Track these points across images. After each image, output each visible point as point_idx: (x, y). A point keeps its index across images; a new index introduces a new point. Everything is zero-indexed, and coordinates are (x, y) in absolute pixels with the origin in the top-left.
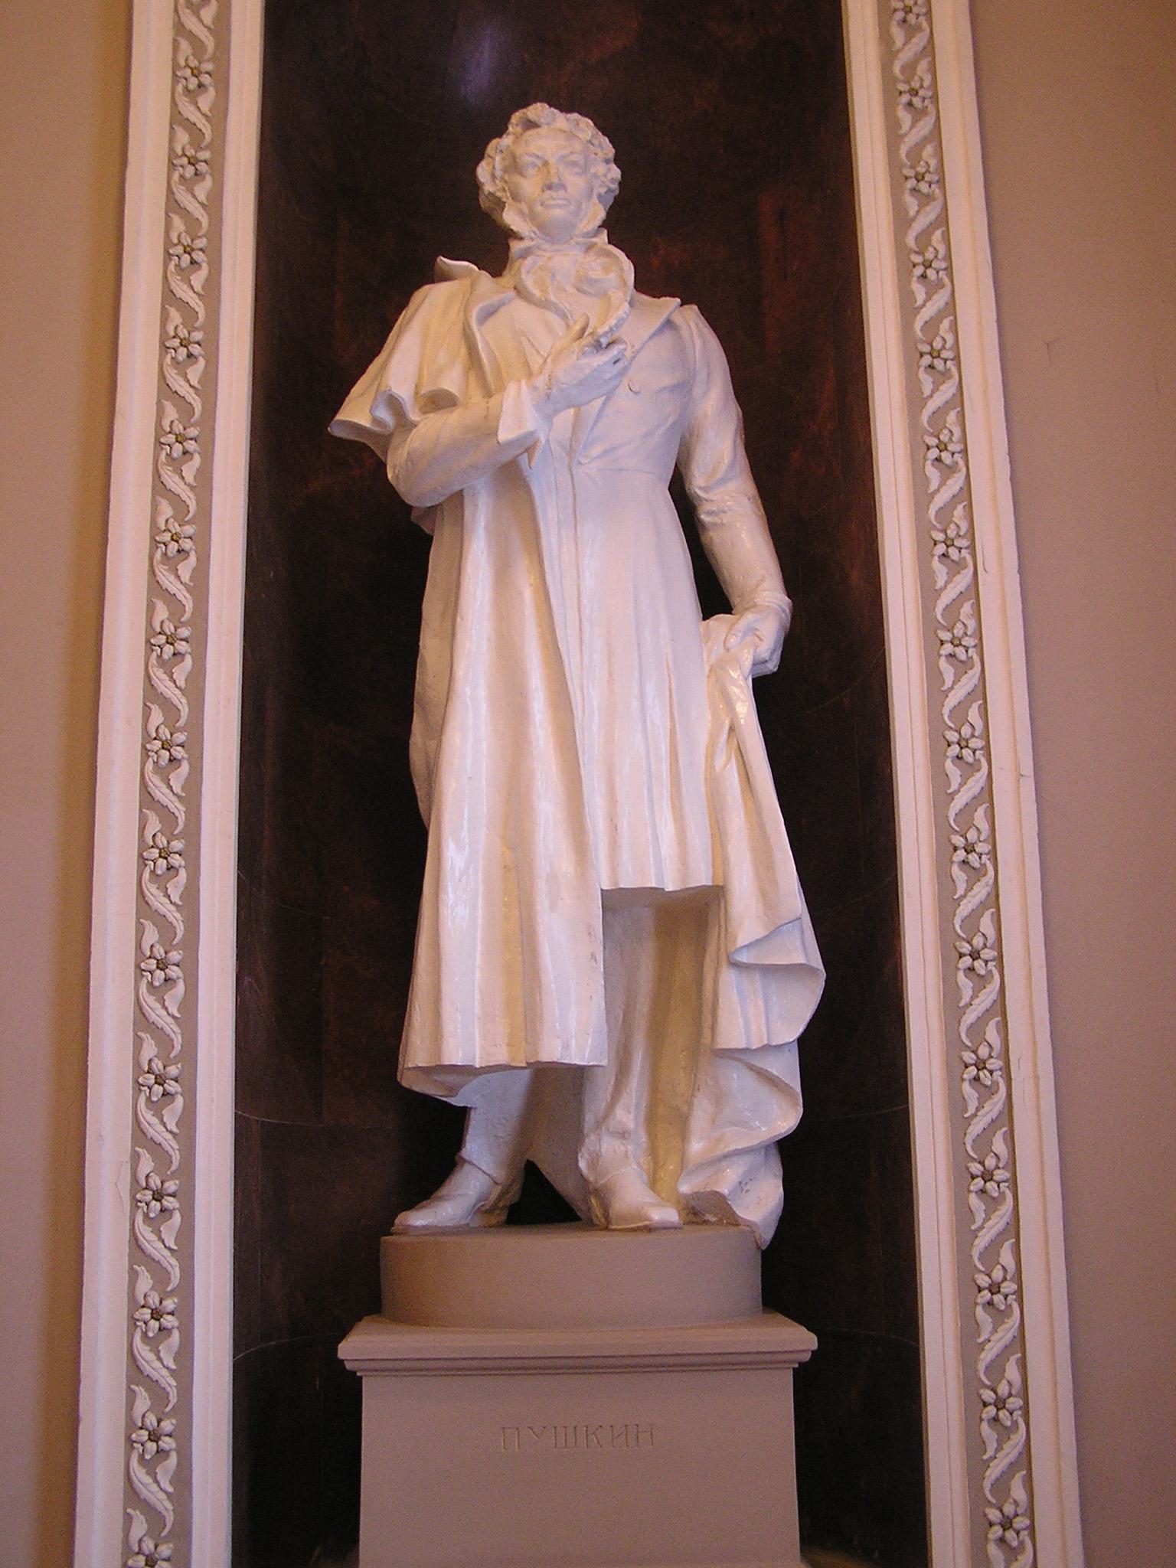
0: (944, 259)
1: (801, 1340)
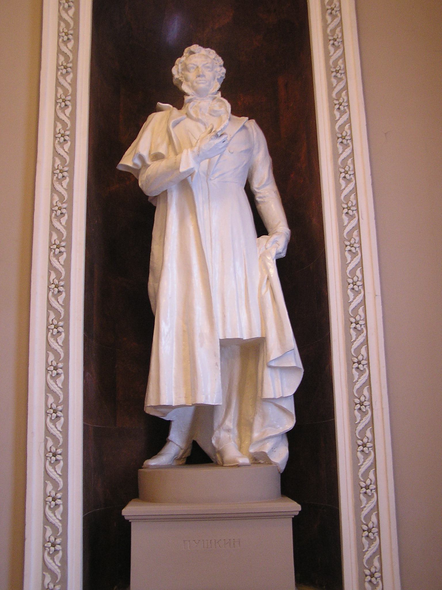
0: (374, 484)
1: (295, 507)
